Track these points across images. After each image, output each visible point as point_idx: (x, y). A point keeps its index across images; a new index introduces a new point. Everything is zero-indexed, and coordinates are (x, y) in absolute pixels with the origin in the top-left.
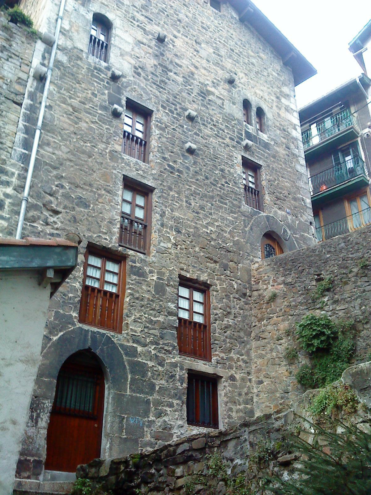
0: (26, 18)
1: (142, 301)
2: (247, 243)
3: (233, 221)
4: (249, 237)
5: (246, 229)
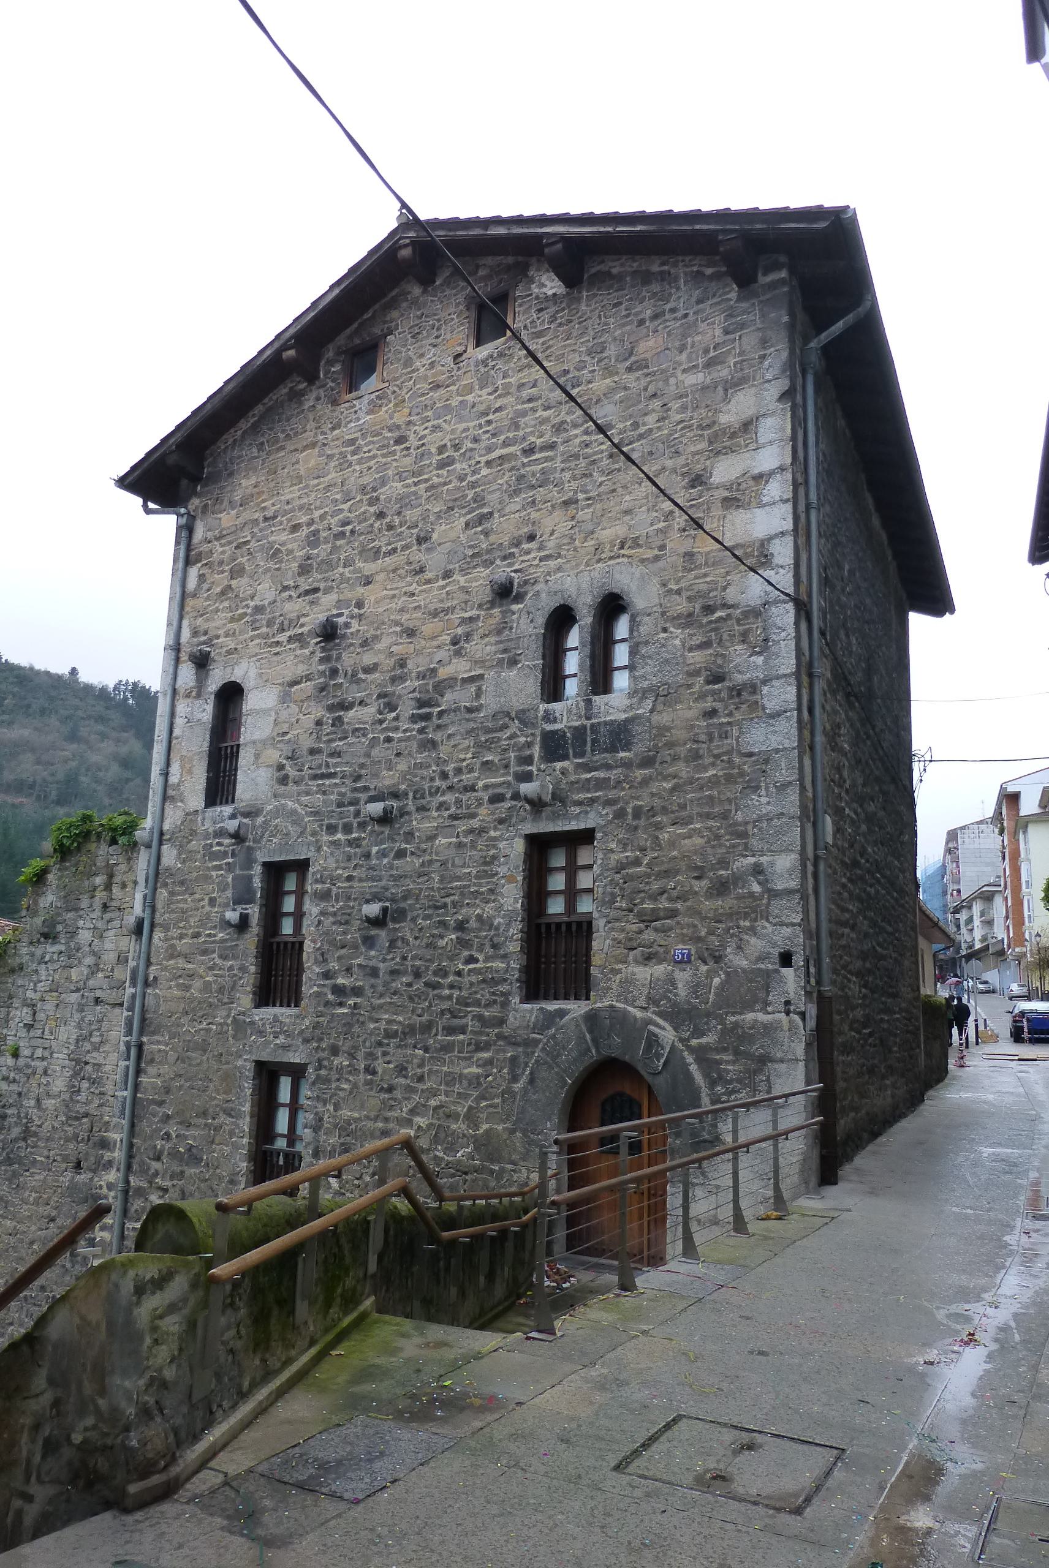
0: (818, 1146)
1: (726, 738)
2: (512, 1132)
3: (478, 1076)
4: (523, 1111)
5: (517, 1087)
